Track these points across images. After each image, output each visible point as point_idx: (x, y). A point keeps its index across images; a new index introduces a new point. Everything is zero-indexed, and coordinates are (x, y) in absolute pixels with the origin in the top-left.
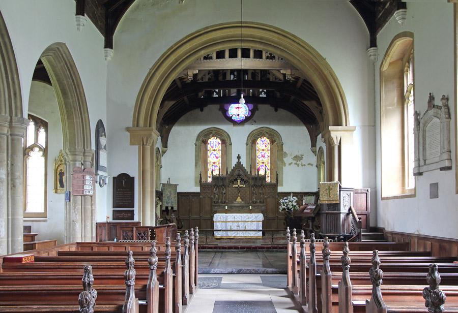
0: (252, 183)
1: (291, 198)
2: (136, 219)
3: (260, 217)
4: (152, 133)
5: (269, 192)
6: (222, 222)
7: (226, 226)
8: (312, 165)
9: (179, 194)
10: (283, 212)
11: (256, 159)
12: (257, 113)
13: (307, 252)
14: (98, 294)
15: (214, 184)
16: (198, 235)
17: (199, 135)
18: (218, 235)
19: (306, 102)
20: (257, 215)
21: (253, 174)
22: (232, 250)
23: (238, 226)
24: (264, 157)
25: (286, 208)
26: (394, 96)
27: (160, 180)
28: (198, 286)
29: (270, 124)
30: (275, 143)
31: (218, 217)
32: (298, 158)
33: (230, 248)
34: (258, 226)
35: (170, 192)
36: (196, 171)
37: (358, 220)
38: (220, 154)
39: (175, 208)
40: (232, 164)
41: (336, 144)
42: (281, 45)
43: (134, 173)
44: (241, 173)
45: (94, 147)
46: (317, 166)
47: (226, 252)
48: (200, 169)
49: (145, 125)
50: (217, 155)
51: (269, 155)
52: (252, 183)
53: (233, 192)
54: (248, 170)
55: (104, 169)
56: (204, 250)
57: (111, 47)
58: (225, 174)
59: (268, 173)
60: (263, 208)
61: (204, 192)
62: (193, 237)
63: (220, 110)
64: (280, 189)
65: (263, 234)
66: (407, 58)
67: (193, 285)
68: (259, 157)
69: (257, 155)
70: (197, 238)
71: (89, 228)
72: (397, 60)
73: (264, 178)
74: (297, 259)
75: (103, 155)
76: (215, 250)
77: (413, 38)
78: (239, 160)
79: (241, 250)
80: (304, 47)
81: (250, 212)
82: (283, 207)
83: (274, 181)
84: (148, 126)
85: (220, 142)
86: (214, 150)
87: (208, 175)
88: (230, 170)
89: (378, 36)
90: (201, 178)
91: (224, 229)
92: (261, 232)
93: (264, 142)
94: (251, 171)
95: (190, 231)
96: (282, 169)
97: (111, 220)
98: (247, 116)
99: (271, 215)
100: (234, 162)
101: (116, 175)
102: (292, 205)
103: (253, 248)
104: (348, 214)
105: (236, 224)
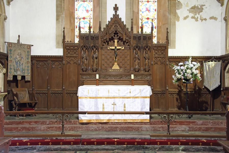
0: (133, 43)
1: (190, 64)
3: (147, 90)
6: (91, 98)
7: (96, 105)
8: (215, 19)
9: (34, 58)
10: (177, 83)
11: (138, 13)
15: (82, 45)
21: (135, 32)
22: (103, 146)
23: (114, 104)
25: (183, 77)
32: (196, 9)
34: (143, 105)
35: (20, 55)
36: (57, 28)
38: (92, 7)
40: (106, 18)
44: (119, 29)
48: (64, 23)
51: (156, 8)
52: (133, 43)
53: (109, 57)
54: (129, 26)
58: (97, 31)
59: (155, 30)
61: (69, 55)
64: (172, 53)
68: (143, 11)
73: (150, 37)
76: (75, 146)
78: (116, 12)
81: (132, 83)
82: (179, 76)
83: (163, 42)
88: (103, 26)
89: (89, 26)
90: (64, 37)
100: (110, 14)
103: (139, 143)
105: (112, 101)
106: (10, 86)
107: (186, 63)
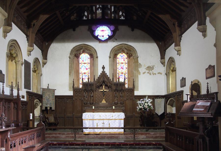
0: (114, 88)
1: (147, 100)
3: (122, 115)
5: (127, 95)
6: (90, 120)
7: (93, 124)
8: (161, 74)
11: (116, 70)
12: (117, 32)
17: (72, 50)
18: (86, 131)
19: (161, 16)
20: (119, 113)
21: (115, 81)
22: (98, 147)
23: (103, 123)
24: (123, 68)
25: (143, 108)
27: (40, 85)
29: (128, 42)
30: (132, 57)
31: (86, 116)
32: (150, 68)
33: (96, 144)
34: (120, 124)
38: (89, 67)
39: (53, 108)
44: (106, 80)
46: (166, 74)
47: (92, 148)
48: (73, 76)
50: (87, 67)
51: (127, 67)
52: (114, 88)
54: (111, 78)
56: (72, 147)
58: (93, 81)
59: (126, 81)
60: (123, 108)
63: (88, 30)
64: (136, 93)
69: (118, 67)
73: (124, 84)
76: (82, 146)
78: (103, 70)
79: (106, 147)
81: (114, 111)
83: (131, 87)
85: (89, 57)
86: (85, 63)
87: (80, 82)
88: (96, 78)
91: (91, 126)
92: (123, 130)
93: (123, 57)
94: (113, 79)
96: (138, 77)
98: (110, 35)
99: (129, 114)
100: (100, 71)
102: (148, 105)
103: (118, 145)
105: (102, 121)
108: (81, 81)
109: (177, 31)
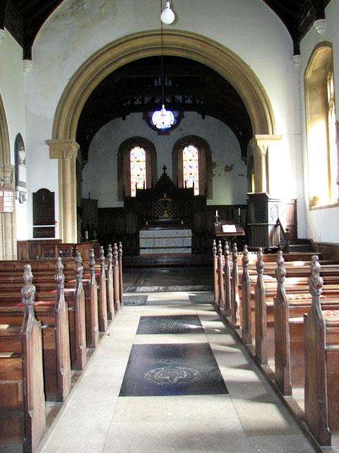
2: (57, 237)
4: (72, 145)
13: (230, 263)
14: (20, 291)
16: (121, 250)
26: (318, 103)
28: (122, 304)
31: (143, 233)
37: (285, 231)
41: (263, 152)
42: (205, 53)
43: (54, 187)
45: (13, 162)
49: (65, 138)
54: (175, 183)
55: (23, 185)
57: (30, 58)
59: (197, 185)
62: (117, 252)
64: (209, 202)
65: (193, 250)
66: (328, 66)
67: (118, 302)
70: (121, 254)
71: (10, 246)
72: (320, 68)
73: (192, 189)
74: (223, 272)
75: (22, 169)
77: (332, 47)
80: (228, 55)
84: (68, 137)
87: (132, 188)
89: (301, 44)
91: (151, 246)
92: (190, 249)
95: (113, 247)
97: (31, 238)
100: (160, 173)
101: (35, 191)
104: (276, 226)
106: (299, 54)
107: (25, 250)
108: (133, 187)
109: (12, 382)
